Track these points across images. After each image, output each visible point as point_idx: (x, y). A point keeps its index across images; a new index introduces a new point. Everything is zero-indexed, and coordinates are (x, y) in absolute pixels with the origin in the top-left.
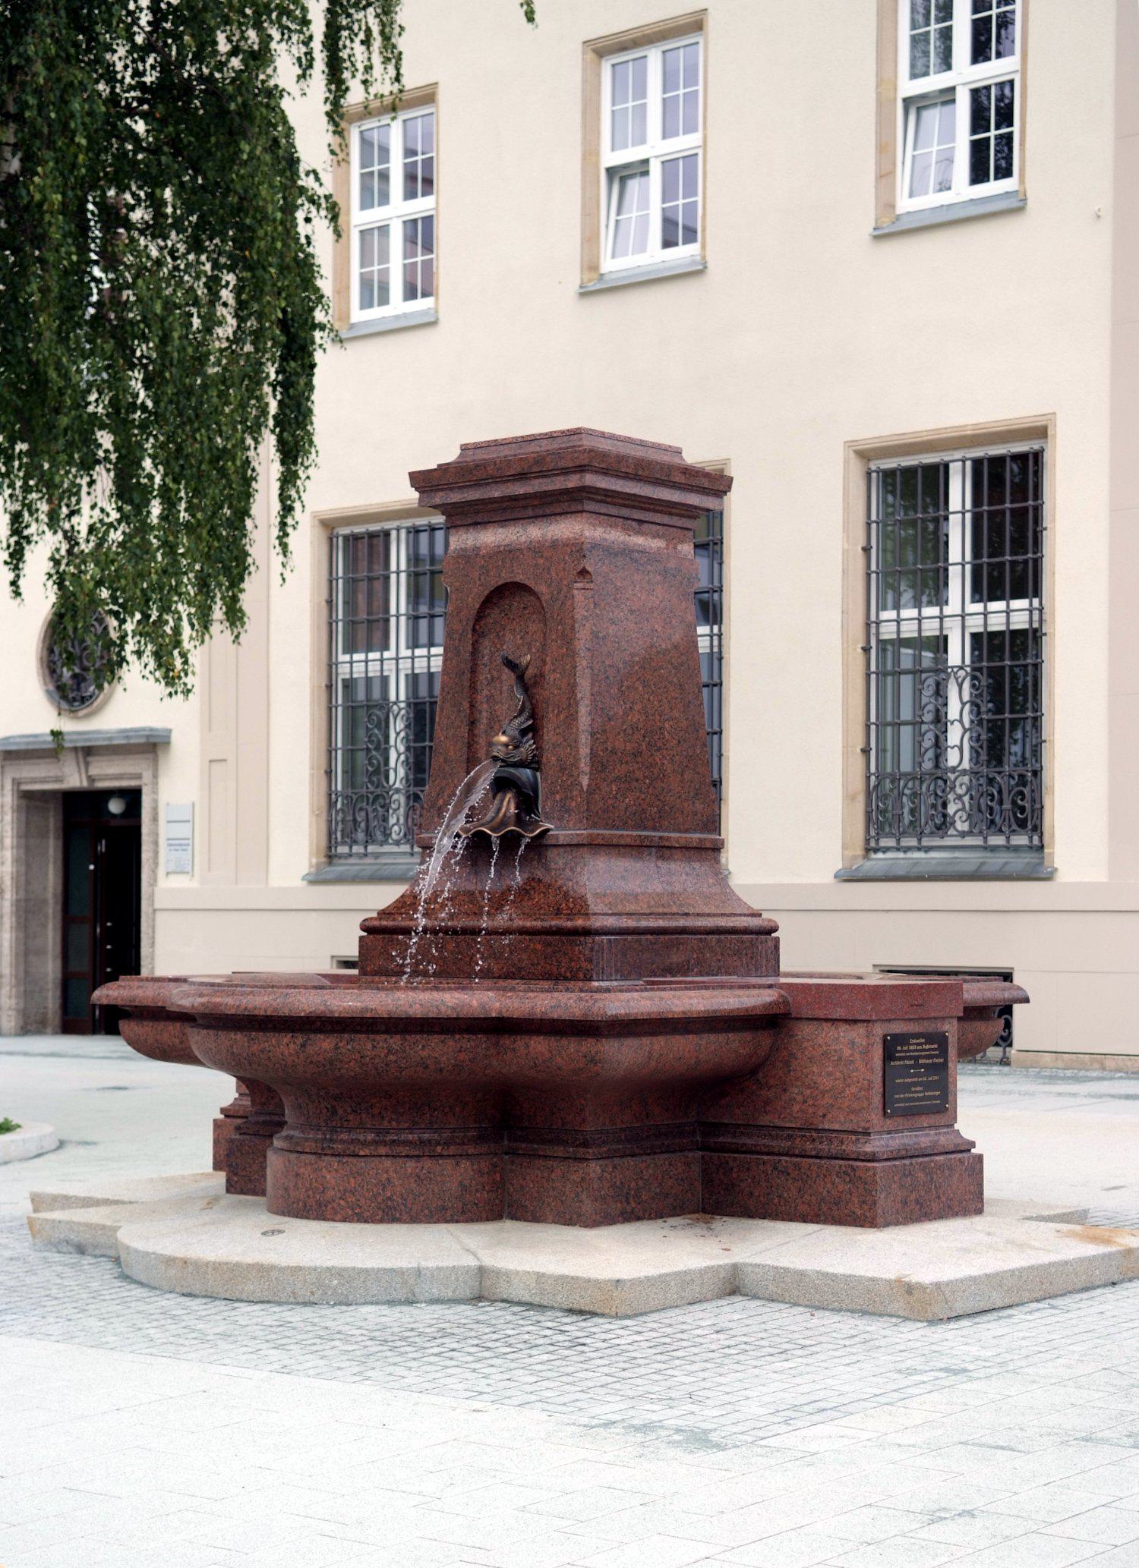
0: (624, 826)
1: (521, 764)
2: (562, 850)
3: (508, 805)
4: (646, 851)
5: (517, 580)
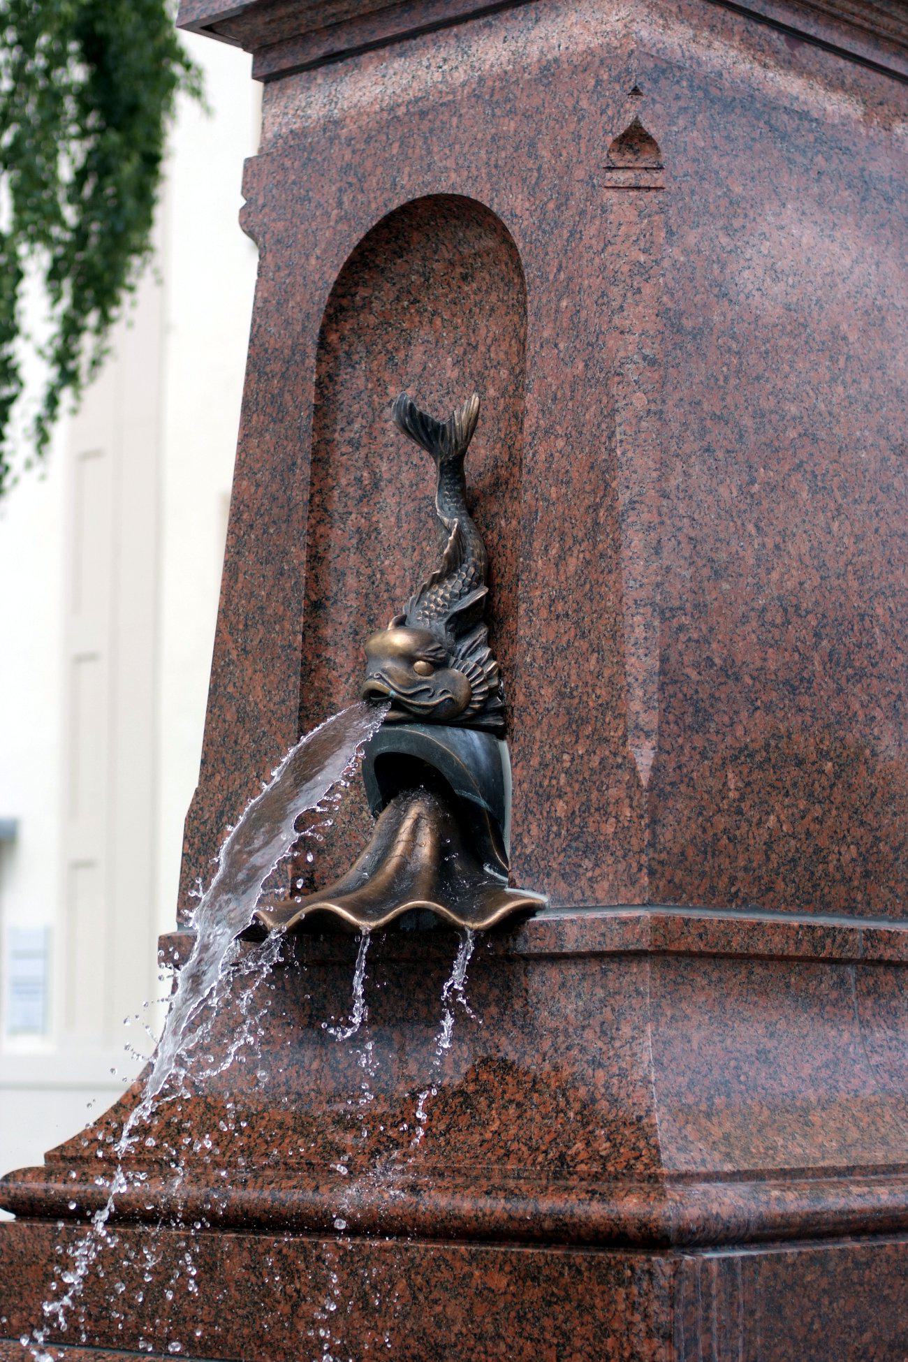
0: (765, 897)
1: (453, 716)
2: (573, 971)
3: (414, 833)
4: (829, 976)
5: (443, 188)
